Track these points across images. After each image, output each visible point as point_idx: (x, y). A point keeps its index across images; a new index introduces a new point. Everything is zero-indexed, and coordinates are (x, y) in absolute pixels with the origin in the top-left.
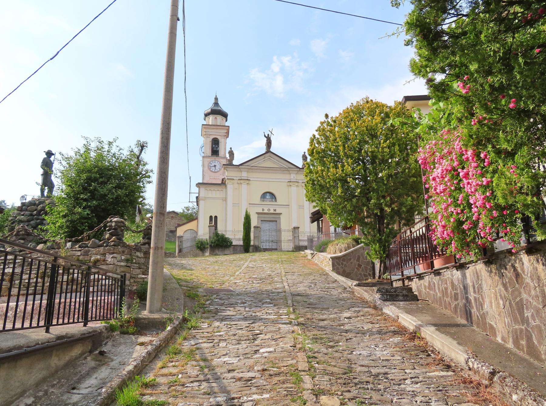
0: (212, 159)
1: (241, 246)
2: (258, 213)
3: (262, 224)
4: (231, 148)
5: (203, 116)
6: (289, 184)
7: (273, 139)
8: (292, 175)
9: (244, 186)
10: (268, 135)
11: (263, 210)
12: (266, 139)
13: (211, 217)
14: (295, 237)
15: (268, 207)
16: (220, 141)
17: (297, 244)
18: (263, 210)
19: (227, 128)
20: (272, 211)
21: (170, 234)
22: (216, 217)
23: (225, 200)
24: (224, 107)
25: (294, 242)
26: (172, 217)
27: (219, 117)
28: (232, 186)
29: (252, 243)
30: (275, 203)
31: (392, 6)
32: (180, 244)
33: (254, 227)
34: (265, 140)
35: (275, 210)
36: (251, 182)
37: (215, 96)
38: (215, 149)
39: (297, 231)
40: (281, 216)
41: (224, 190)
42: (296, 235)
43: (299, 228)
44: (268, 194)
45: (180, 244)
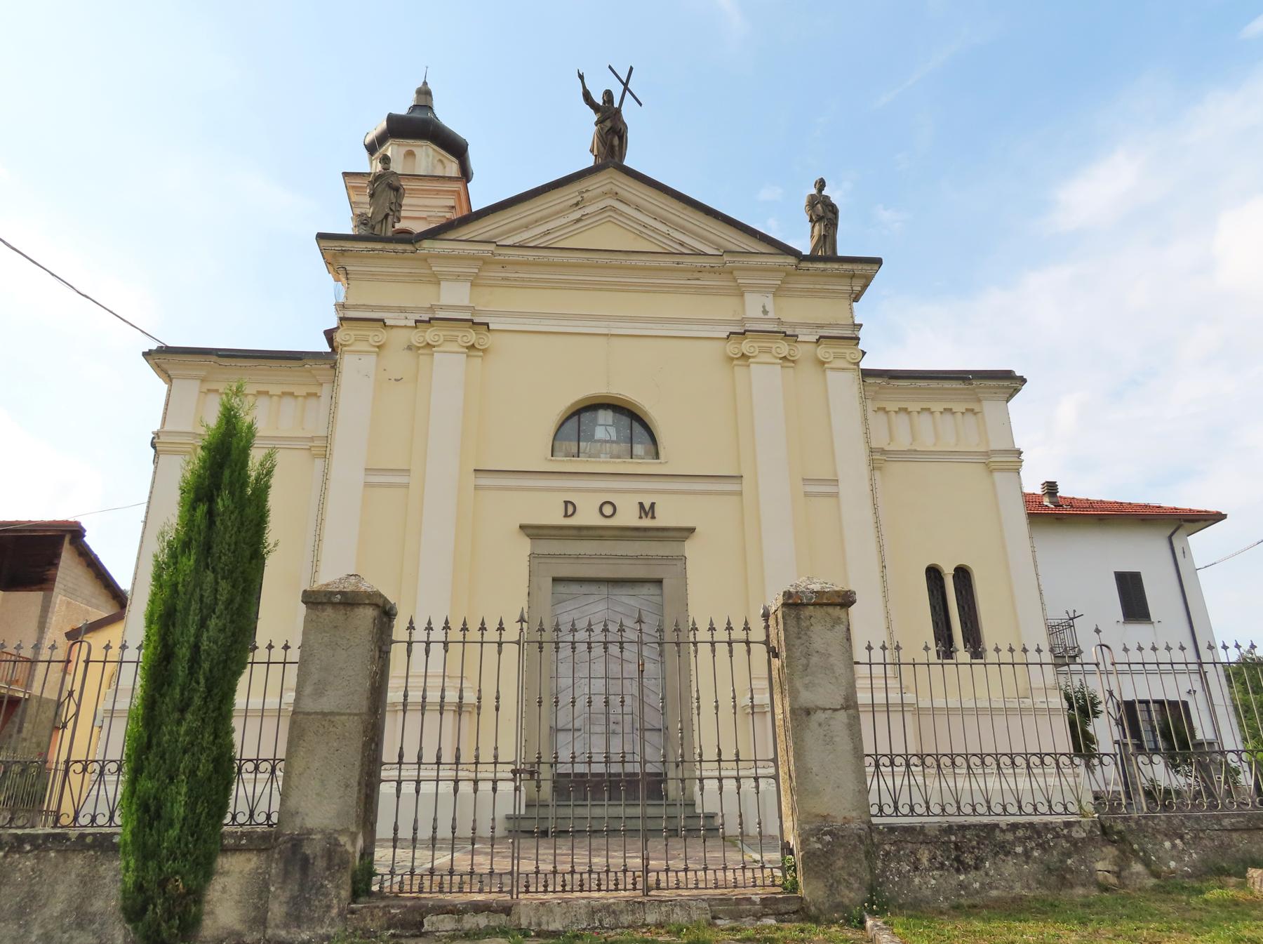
1: (103, 844)
2: (532, 532)
3: (557, 602)
6: (732, 348)
7: (629, 113)
8: (748, 297)
9: (449, 366)
10: (608, 95)
11: (570, 508)
12: (593, 117)
14: (802, 714)
15: (605, 490)
17: (836, 804)
18: (570, 508)
20: (628, 516)
24: (447, 115)
25: (803, 784)
29: (253, 797)
30: (651, 467)
31: (864, 353)
33: (314, 600)
35: (647, 511)
36: (488, 340)
37: (420, 85)
39: (821, 636)
40: (691, 549)
42: (824, 694)
43: (846, 600)
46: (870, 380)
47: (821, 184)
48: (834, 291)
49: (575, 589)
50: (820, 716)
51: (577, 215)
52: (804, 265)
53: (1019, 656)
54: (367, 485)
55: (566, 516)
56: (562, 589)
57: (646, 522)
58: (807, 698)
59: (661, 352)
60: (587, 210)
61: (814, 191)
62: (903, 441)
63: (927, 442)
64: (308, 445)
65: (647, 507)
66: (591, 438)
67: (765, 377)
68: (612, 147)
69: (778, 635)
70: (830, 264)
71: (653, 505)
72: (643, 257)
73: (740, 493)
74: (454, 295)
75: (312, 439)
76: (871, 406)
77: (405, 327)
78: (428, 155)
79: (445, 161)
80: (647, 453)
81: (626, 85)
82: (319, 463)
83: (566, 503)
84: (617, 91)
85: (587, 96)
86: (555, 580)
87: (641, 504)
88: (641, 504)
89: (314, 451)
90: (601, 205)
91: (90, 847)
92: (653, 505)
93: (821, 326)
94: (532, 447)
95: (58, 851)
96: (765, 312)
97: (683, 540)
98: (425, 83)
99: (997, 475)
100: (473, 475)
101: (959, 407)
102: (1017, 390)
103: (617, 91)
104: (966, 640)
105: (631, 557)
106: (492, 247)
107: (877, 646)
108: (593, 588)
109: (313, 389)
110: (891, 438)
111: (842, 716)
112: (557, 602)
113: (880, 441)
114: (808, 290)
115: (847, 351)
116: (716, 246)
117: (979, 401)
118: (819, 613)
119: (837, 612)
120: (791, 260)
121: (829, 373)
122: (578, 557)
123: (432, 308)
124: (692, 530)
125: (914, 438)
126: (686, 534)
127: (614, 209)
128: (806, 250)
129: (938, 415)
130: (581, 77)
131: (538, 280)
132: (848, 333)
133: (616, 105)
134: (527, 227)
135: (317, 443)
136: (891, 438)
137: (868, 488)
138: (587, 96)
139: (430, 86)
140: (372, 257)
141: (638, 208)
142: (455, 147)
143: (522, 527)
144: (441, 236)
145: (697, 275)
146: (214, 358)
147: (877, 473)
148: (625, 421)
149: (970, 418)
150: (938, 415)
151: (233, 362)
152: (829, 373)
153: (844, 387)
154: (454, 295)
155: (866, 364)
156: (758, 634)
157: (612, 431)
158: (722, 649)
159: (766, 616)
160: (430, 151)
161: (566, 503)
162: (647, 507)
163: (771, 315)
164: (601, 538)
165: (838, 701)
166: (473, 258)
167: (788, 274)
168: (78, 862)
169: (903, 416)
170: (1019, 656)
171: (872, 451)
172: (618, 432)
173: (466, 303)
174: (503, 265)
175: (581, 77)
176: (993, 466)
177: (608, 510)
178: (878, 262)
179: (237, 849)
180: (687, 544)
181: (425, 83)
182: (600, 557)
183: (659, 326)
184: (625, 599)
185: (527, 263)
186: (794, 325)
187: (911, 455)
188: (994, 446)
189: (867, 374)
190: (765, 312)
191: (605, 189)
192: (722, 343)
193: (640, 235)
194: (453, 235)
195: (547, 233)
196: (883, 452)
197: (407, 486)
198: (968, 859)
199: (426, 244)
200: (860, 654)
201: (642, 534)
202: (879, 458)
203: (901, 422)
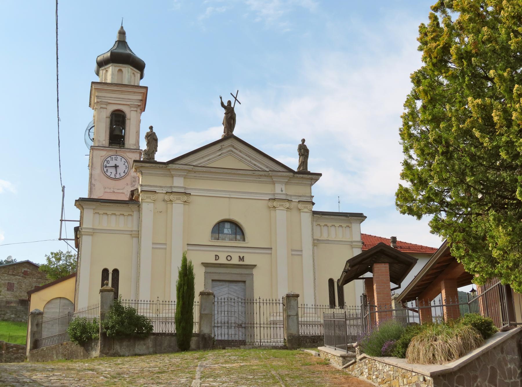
0: (111, 153)
1: (171, 335)
3: (213, 287)
4: (151, 128)
5: (95, 65)
6: (270, 204)
7: (238, 109)
8: (276, 184)
9: (178, 208)
10: (229, 102)
11: (217, 257)
12: (223, 111)
13: (105, 272)
14: (288, 316)
17: (294, 332)
18: (217, 257)
19: (143, 90)
20: (235, 261)
22: (116, 272)
23: (137, 235)
24: (137, 48)
26: (25, 273)
27: (128, 71)
29: (196, 329)
30: (242, 244)
32: (35, 329)
35: (241, 259)
37: (119, 28)
40: (255, 271)
41: (135, 214)
42: (293, 313)
43: (298, 296)
44: (227, 225)
45: (35, 329)
46: (315, 216)
47: (303, 141)
48: (305, 184)
49: (218, 283)
50: (292, 317)
51: (219, 153)
52: (296, 175)
53: (164, 303)
54: (153, 248)
55: (216, 260)
56: (215, 283)
57: (241, 263)
58: (289, 313)
59: (246, 203)
60: (223, 151)
62: (325, 237)
63: (333, 237)
65: (241, 257)
67: (281, 215)
68: (231, 124)
69: (285, 301)
70: (305, 175)
71: (243, 257)
73: (271, 254)
74: (178, 183)
75: (132, 231)
76: (315, 224)
78: (128, 72)
79: (135, 73)
80: (241, 238)
81: (236, 98)
82: (135, 240)
83: (216, 255)
84: (233, 100)
85: (222, 104)
86: (213, 280)
89: (133, 235)
90: (228, 149)
92: (243, 257)
93: (300, 196)
94: (204, 235)
96: (282, 191)
97: (253, 268)
98: (122, 27)
99: (354, 249)
100: (186, 246)
101: (344, 225)
102: (363, 220)
103: (233, 100)
105: (236, 274)
106: (192, 167)
108: (224, 283)
109: (130, 213)
110: (321, 235)
111: (296, 317)
112: (213, 287)
113: (317, 236)
115: (309, 206)
116: (266, 167)
118: (292, 298)
119: (296, 298)
120: (292, 174)
122: (220, 273)
123: (171, 187)
124: (255, 266)
125: (329, 236)
128: (296, 170)
129: (337, 227)
130: (221, 98)
131: (207, 177)
133: (232, 106)
135: (134, 233)
136: (321, 235)
137: (312, 253)
138: (222, 104)
139: (125, 29)
141: (240, 151)
142: (139, 66)
143: (202, 263)
144: (177, 163)
145: (260, 177)
147: (315, 247)
148: (234, 227)
149: (348, 229)
150: (337, 227)
152: (302, 213)
153: (306, 218)
155: (315, 208)
156: (281, 301)
157: (230, 230)
158: (268, 304)
159: (283, 298)
160: (130, 69)
161: (216, 255)
162: (241, 257)
163: (284, 192)
164: (227, 267)
165: (295, 314)
166: (186, 170)
167: (290, 178)
168: (168, 337)
169: (326, 227)
170: (321, 307)
171: (314, 240)
172: (232, 231)
173: (182, 185)
174: (195, 172)
175: (221, 98)
176: (353, 246)
177: (229, 258)
178: (320, 175)
179: (194, 336)
180: (254, 270)
181: (122, 27)
182: (226, 273)
184: (233, 287)
185: (203, 172)
186: (291, 196)
187: (327, 242)
188: (354, 240)
189: (315, 213)
190: (282, 191)
192: (267, 202)
194: (179, 162)
196: (318, 240)
197: (166, 249)
198: (315, 341)
199: (170, 165)
200: (300, 306)
202: (316, 242)
203: (325, 229)
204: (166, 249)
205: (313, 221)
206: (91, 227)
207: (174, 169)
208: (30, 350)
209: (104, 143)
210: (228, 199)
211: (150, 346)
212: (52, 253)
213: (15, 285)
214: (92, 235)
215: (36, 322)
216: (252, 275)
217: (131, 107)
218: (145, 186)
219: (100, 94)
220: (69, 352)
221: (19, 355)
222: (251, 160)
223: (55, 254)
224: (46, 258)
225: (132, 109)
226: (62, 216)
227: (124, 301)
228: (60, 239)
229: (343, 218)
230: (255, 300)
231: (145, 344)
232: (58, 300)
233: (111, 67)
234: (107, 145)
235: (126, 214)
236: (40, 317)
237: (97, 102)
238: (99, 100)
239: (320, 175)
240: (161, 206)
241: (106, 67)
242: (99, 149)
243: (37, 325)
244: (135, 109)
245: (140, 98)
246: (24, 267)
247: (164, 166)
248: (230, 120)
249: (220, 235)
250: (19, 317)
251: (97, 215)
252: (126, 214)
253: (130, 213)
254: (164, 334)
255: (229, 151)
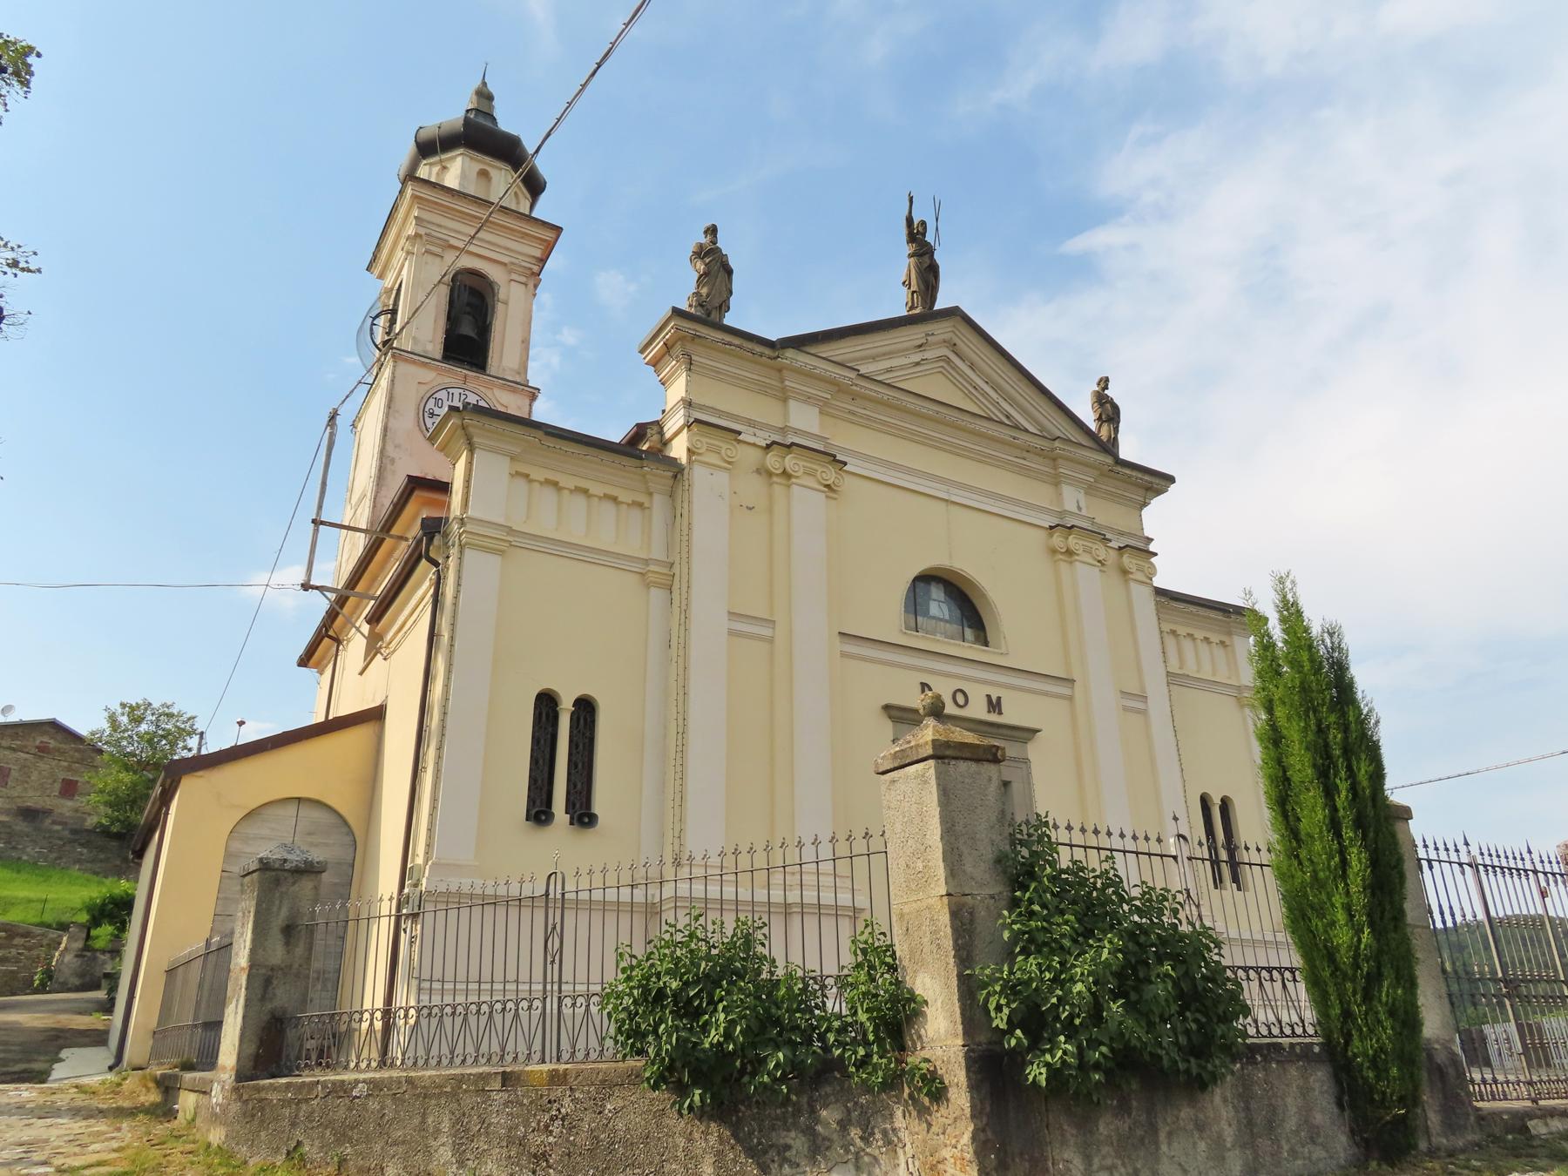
0: (447, 380)
1: (1303, 1054)
4: (712, 231)
5: (409, 148)
6: (1057, 540)
8: (793, 405)
9: (805, 502)
13: (546, 704)
16: (502, 295)
19: (548, 235)
21: (21, 826)
22: (586, 709)
23: (666, 577)
26: (43, 750)
27: (502, 180)
28: (722, 478)
32: (276, 953)
34: (901, 261)
36: (848, 484)
37: (477, 83)
38: (467, 329)
40: (1033, 751)
41: (659, 503)
44: (937, 592)
45: (276, 953)
51: (916, 358)
57: (993, 718)
60: (928, 355)
61: (703, 240)
64: (637, 567)
66: (926, 614)
71: (999, 698)
72: (967, 418)
75: (646, 562)
76: (1166, 627)
77: (754, 445)
82: (657, 595)
85: (910, 220)
87: (989, 697)
88: (989, 697)
89: (651, 577)
91: (1299, 1057)
92: (999, 698)
95: (1278, 1062)
96: (1079, 508)
104: (570, 807)
106: (853, 375)
107: (825, 837)
109: (642, 498)
114: (1112, 494)
117: (1230, 634)
121: (1133, 585)
126: (1025, 735)
127: (948, 361)
131: (884, 423)
132: (1140, 545)
134: (874, 358)
140: (728, 353)
141: (972, 366)
143: (887, 708)
144: (808, 349)
145: (1025, 454)
146: (540, 434)
151: (559, 444)
154: (804, 419)
157: (945, 607)
163: (1084, 512)
166: (832, 382)
178: (1171, 479)
180: (1030, 746)
181: (484, 84)
183: (883, 470)
190: (1079, 508)
191: (947, 336)
193: (968, 395)
194: (827, 350)
195: (889, 370)
199: (790, 353)
201: (994, 730)
204: (771, 640)
205: (1157, 603)
206: (501, 521)
207: (799, 372)
208: (241, 1076)
209: (430, 347)
210: (942, 505)
211: (1229, 1134)
212: (123, 705)
213: (14, 774)
214: (501, 553)
215: (284, 912)
216: (1026, 761)
217: (510, 272)
218: (702, 408)
219: (426, 216)
220: (582, 1139)
221: (14, 951)
222: (1000, 401)
223: (131, 707)
224: (106, 714)
225: (514, 276)
226: (320, 507)
227: (1063, 836)
228: (306, 586)
229: (1212, 614)
230: (1419, 843)
231: (1201, 1127)
232: (291, 810)
233: (459, 159)
234: (439, 355)
235: (624, 496)
236: (306, 886)
237: (417, 235)
238: (422, 231)
239: (1171, 479)
240: (753, 488)
241: (444, 157)
242: (414, 362)
243: (289, 931)
244: (523, 279)
245: (538, 253)
246: (45, 733)
247: (767, 351)
248: (927, 275)
249: (920, 619)
250: (14, 848)
251: (521, 483)
252: (624, 496)
253: (642, 498)
254: (1277, 1047)
255: (940, 358)
